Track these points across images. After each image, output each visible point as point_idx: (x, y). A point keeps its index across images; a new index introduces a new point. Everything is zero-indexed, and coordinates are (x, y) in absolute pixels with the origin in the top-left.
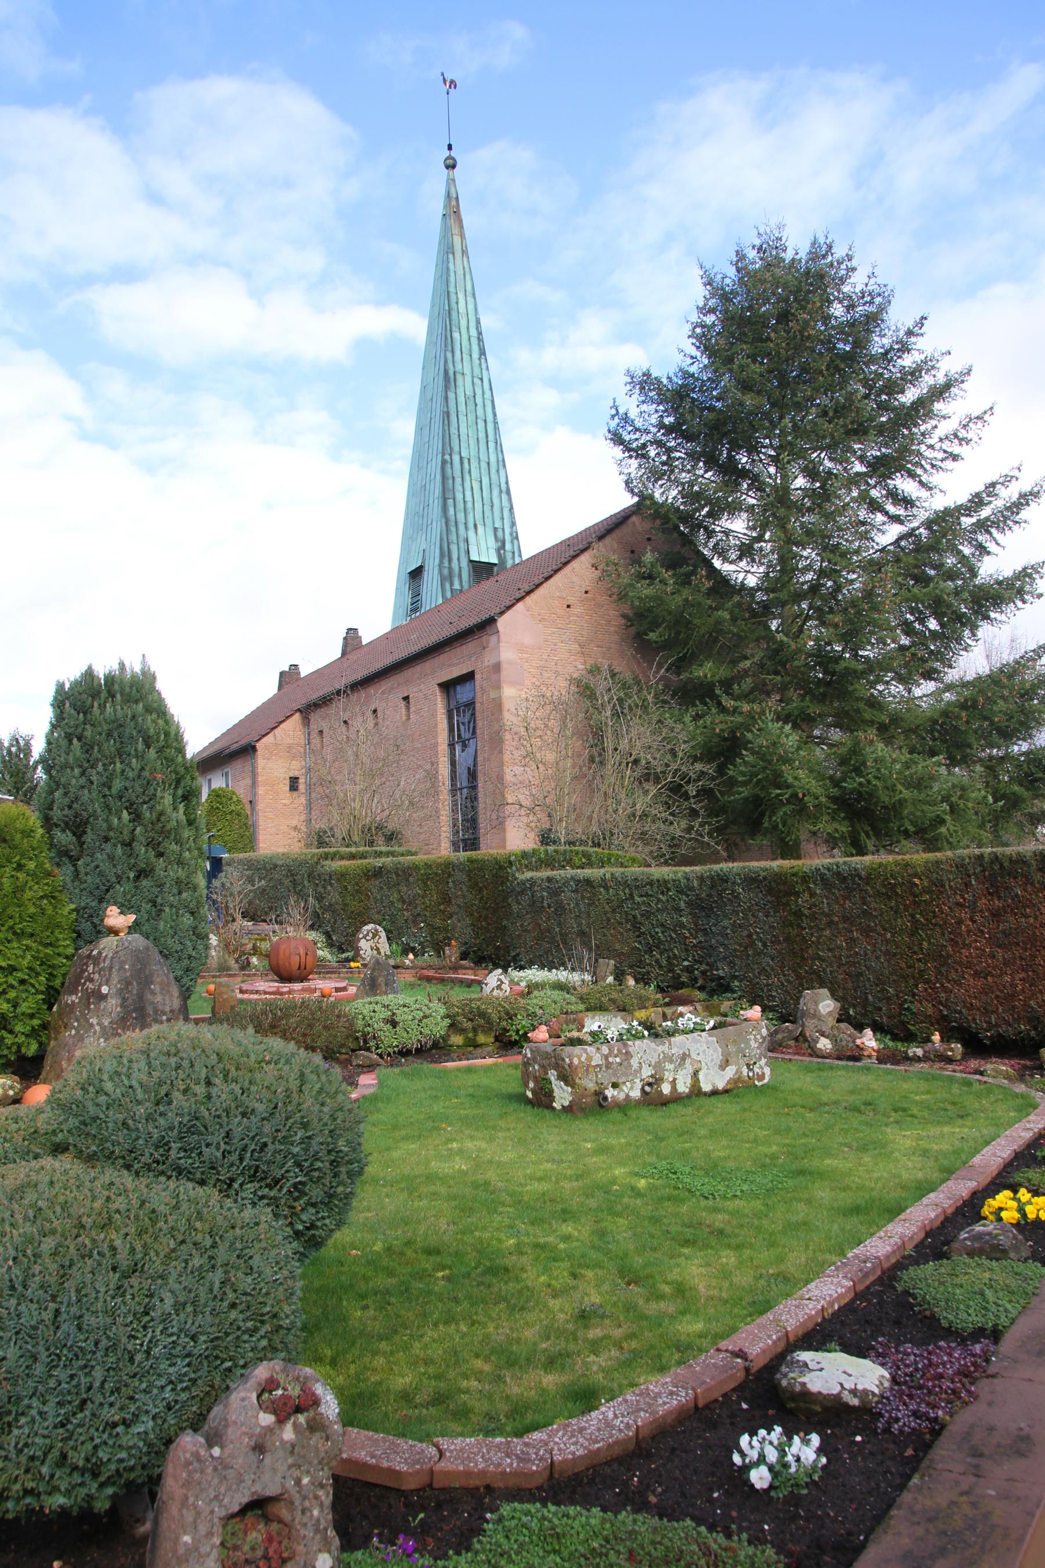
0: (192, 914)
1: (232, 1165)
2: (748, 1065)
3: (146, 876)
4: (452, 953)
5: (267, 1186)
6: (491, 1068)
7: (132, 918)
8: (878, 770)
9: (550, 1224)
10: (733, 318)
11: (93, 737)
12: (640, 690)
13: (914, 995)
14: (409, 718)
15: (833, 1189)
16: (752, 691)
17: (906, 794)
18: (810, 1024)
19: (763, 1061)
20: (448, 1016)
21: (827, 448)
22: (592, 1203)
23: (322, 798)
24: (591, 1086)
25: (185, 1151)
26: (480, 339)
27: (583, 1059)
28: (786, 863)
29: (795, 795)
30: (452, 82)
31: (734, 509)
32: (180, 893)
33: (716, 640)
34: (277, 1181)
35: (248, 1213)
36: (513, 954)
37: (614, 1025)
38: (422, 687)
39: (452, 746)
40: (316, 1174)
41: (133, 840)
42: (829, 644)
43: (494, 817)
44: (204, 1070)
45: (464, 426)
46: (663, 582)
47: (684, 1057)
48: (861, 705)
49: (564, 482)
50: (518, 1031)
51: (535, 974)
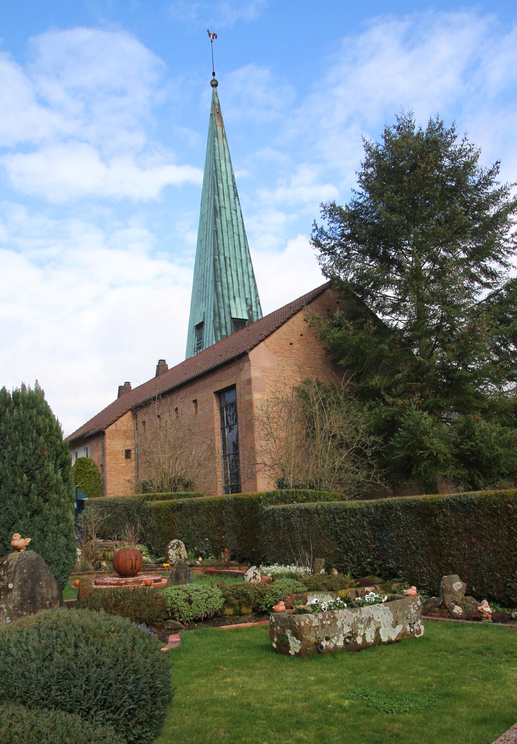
0: (66, 536)
1: (90, 699)
2: (410, 625)
3: (38, 514)
4: (225, 556)
5: (111, 712)
6: (250, 629)
7: (29, 540)
8: (483, 437)
9: (289, 731)
10: (384, 169)
11: (5, 430)
12: (335, 393)
13: (513, 578)
14: (197, 413)
15: (468, 707)
16: (404, 392)
17: (501, 451)
18: (448, 597)
19: (419, 622)
20: (223, 596)
21: (441, 245)
22: (315, 717)
23: (145, 463)
24: (313, 639)
25: (61, 691)
26: (234, 187)
27: (307, 622)
28: (428, 497)
29: (431, 454)
30: (214, 35)
31: (388, 283)
32: (58, 524)
33: (380, 361)
34: (117, 709)
35: (99, 731)
36: (263, 556)
37: (326, 600)
38: (205, 394)
39: (223, 429)
40: (142, 703)
41: (30, 492)
42: (449, 361)
43: (249, 472)
44: (74, 638)
45: (226, 238)
46: (347, 328)
47: (370, 620)
48: (471, 398)
49: (287, 271)
50: (267, 605)
51: (277, 569)
